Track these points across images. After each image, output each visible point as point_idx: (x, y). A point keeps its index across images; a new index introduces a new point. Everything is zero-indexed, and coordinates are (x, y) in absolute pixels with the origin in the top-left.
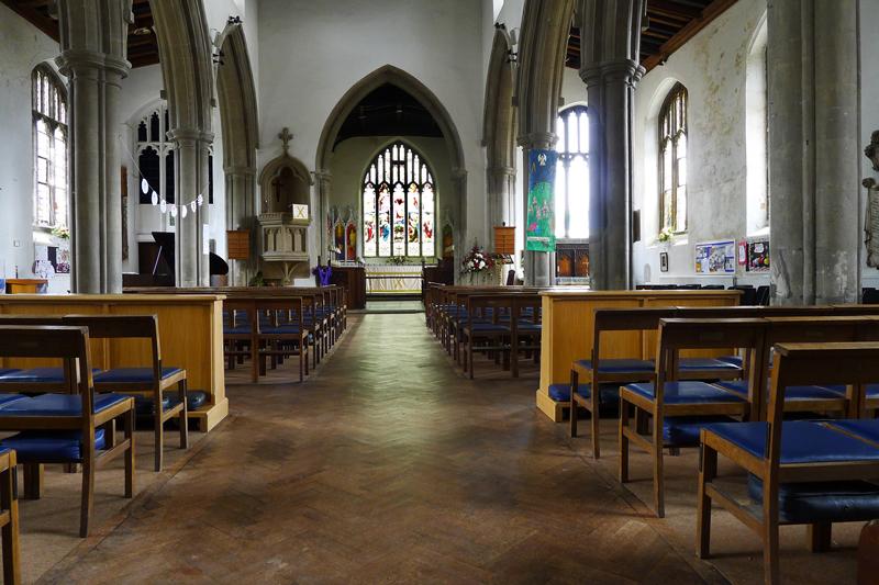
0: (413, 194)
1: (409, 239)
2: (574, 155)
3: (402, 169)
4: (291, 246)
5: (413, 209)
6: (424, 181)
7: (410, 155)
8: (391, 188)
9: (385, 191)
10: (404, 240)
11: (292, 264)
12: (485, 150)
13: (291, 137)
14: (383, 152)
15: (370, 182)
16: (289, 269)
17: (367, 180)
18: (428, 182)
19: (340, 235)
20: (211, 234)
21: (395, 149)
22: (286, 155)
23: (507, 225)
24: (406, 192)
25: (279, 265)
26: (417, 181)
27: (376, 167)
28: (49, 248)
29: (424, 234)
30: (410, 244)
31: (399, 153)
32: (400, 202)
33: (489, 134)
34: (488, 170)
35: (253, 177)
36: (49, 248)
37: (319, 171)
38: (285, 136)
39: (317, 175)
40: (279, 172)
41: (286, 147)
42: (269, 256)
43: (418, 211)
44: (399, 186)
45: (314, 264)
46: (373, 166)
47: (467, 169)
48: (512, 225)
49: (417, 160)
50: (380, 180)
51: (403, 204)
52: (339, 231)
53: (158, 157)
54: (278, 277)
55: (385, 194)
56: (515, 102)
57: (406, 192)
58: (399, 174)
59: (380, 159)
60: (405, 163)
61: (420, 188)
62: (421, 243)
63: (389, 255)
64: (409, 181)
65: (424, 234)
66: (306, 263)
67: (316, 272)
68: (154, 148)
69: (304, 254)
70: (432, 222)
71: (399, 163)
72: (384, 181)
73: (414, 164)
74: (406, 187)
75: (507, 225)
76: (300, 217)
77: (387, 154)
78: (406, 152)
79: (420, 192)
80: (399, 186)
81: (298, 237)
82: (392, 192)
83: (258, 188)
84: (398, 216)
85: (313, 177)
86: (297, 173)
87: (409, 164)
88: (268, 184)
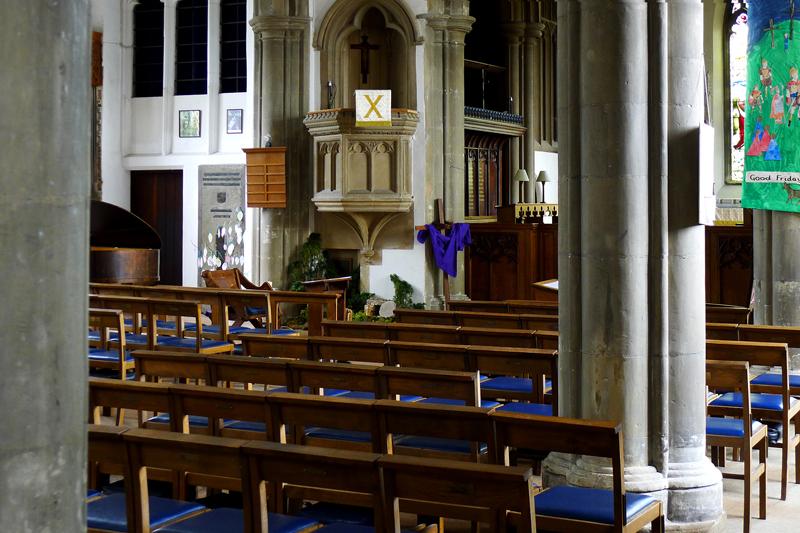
4: (737, 187)
11: (375, 218)
16: (371, 231)
25: (344, 220)
28: (764, 518)
35: (303, 34)
36: (764, 518)
37: (440, 11)
39: (431, 22)
40: (357, 22)
42: (326, 200)
45: (423, 218)
54: (353, 246)
66: (405, 217)
67: (425, 235)
69: (395, 197)
76: (373, 117)
81: (380, 160)
83: (313, 57)
85: (421, 27)
86: (393, 20)
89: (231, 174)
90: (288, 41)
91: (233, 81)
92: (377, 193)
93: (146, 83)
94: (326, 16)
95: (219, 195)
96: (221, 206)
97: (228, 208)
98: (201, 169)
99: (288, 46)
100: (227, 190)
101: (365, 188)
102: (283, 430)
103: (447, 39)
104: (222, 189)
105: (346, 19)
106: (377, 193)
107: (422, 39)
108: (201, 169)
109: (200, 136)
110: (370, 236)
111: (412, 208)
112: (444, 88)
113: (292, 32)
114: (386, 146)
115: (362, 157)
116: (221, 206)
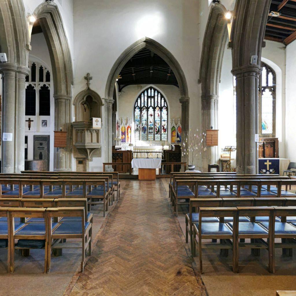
0: (157, 112)
1: (155, 133)
2: (265, 88)
3: (153, 100)
5: (157, 119)
6: (163, 106)
7: (156, 94)
8: (148, 108)
9: (145, 110)
10: (153, 133)
12: (200, 85)
13: (91, 78)
14: (143, 92)
15: (137, 106)
17: (136, 105)
18: (164, 106)
19: (123, 131)
20: (152, 118)
21: (149, 91)
22: (89, 89)
23: (213, 129)
24: (154, 111)
26: (159, 106)
27: (141, 99)
29: (162, 130)
30: (156, 135)
31: (151, 93)
32: (151, 115)
33: (203, 75)
34: (202, 97)
37: (107, 98)
38: (88, 78)
39: (105, 100)
41: (88, 84)
43: (160, 120)
44: (151, 108)
46: (139, 99)
47: (189, 97)
48: (216, 129)
49: (159, 96)
50: (142, 105)
51: (153, 117)
52: (123, 129)
53: (35, 90)
55: (144, 112)
56: (231, 45)
57: (154, 111)
58: (151, 102)
59: (142, 96)
60: (154, 97)
61: (161, 109)
62: (161, 135)
63: (82, 249)
64: (156, 105)
65: (162, 130)
68: (33, 85)
69: (98, 144)
70: (166, 125)
71: (151, 97)
72: (144, 106)
73: (158, 98)
74: (154, 108)
75: (213, 129)
77: (146, 93)
78: (154, 92)
79: (161, 111)
80: (151, 108)
82: (148, 111)
83: (73, 107)
84: (150, 122)
85: (103, 101)
87: (156, 98)
88: (79, 105)
89: (44, 138)
90: (66, 102)
91: (199, 213)
92: (94, 143)
93: (30, 111)
94: (76, 96)
95: (40, 143)
96: (41, 146)
97: (43, 147)
98: (34, 136)
99: (66, 103)
100: (43, 142)
101: (90, 142)
102: (62, 186)
103: (109, 105)
104: (41, 142)
105: (82, 98)
106: (94, 143)
107: (104, 104)
108: (34, 136)
109: (47, 120)
110: (90, 154)
111: (101, 147)
112: (108, 117)
113: (67, 100)
114: (96, 131)
115: (90, 133)
116: (41, 146)
